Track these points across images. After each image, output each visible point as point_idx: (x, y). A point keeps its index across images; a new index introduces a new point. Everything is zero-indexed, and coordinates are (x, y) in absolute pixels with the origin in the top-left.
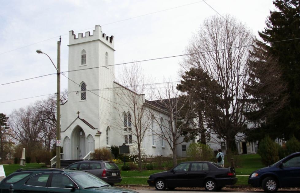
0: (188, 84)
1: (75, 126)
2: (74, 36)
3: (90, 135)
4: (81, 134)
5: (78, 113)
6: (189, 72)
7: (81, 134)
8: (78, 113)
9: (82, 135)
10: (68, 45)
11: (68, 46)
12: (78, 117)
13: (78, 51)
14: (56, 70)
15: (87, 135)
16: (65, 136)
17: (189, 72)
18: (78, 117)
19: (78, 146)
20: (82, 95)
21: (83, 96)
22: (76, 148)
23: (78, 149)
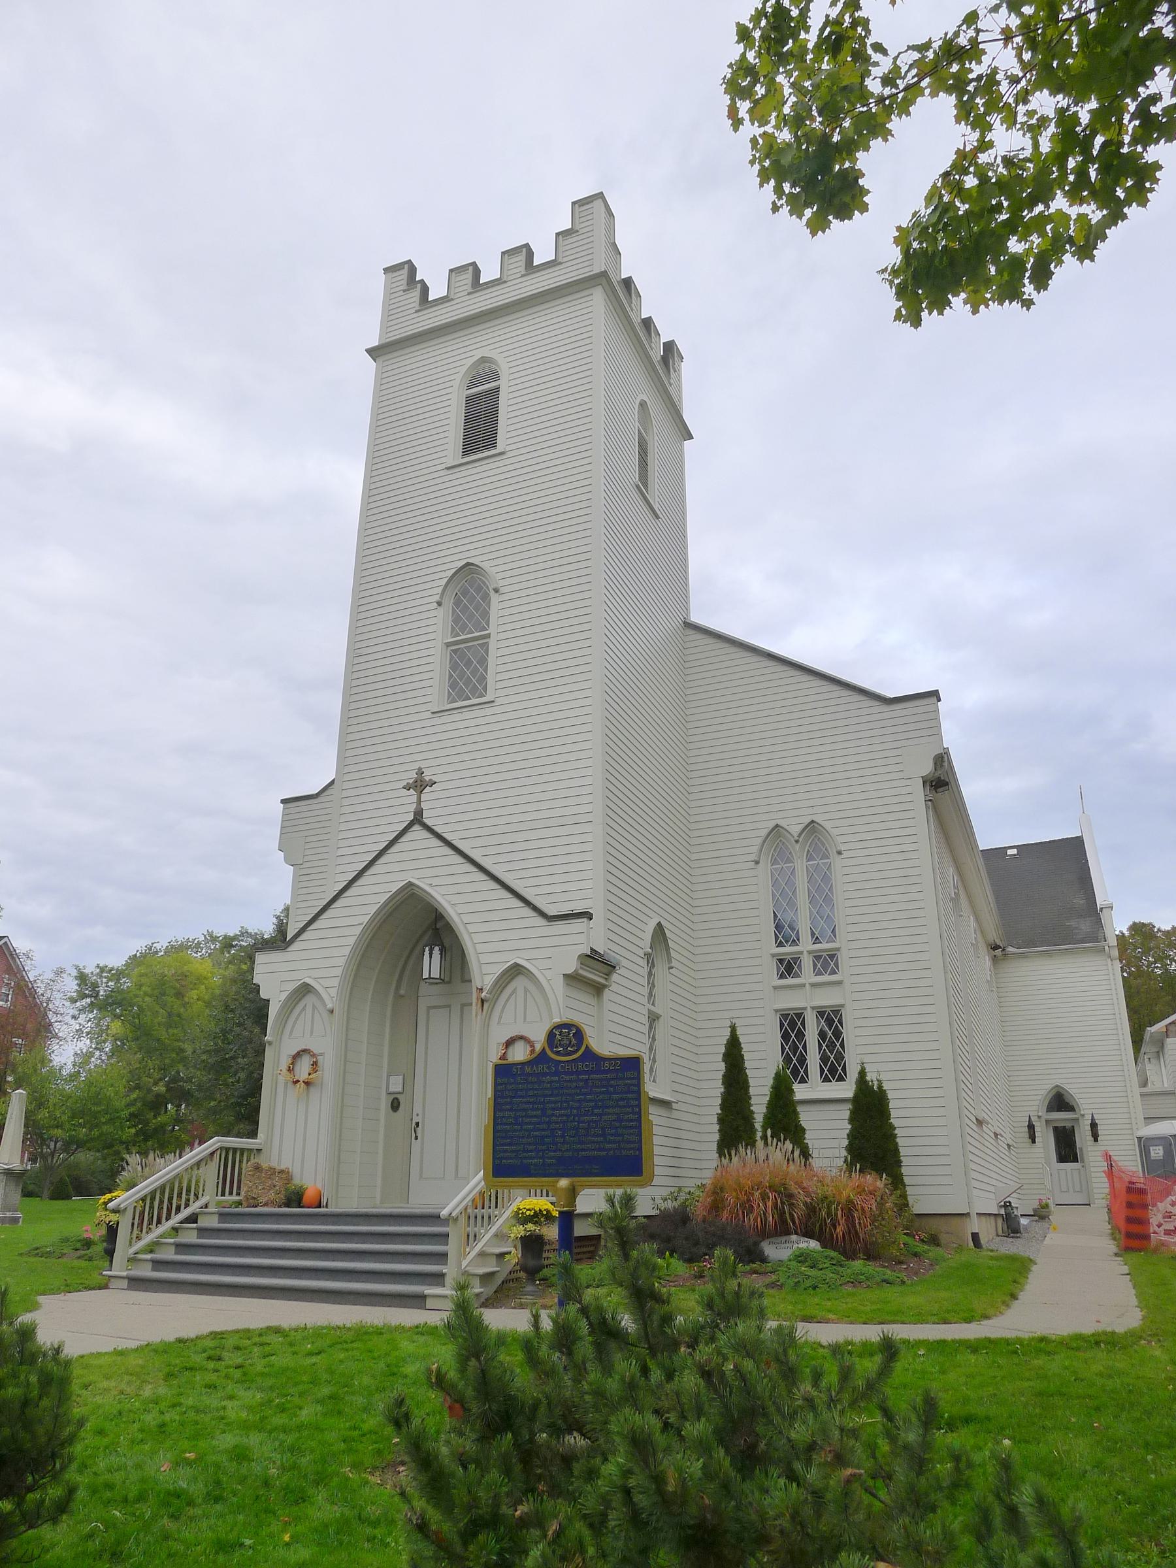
0: (912, 1489)
1: (383, 898)
2: (416, 293)
3: (516, 971)
4: (432, 964)
5: (420, 785)
6: (1126, 933)
7: (436, 974)
8: (420, 785)
9: (442, 980)
10: (375, 343)
11: (369, 351)
12: (418, 819)
13: (445, 375)
14: (193, 1336)
15: (485, 969)
16: (292, 986)
17: (1126, 933)
18: (418, 819)
19: (396, 1085)
20: (454, 666)
21: (462, 675)
22: (384, 1103)
23: (395, 1105)
